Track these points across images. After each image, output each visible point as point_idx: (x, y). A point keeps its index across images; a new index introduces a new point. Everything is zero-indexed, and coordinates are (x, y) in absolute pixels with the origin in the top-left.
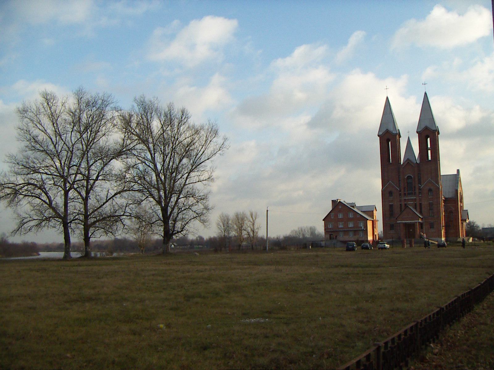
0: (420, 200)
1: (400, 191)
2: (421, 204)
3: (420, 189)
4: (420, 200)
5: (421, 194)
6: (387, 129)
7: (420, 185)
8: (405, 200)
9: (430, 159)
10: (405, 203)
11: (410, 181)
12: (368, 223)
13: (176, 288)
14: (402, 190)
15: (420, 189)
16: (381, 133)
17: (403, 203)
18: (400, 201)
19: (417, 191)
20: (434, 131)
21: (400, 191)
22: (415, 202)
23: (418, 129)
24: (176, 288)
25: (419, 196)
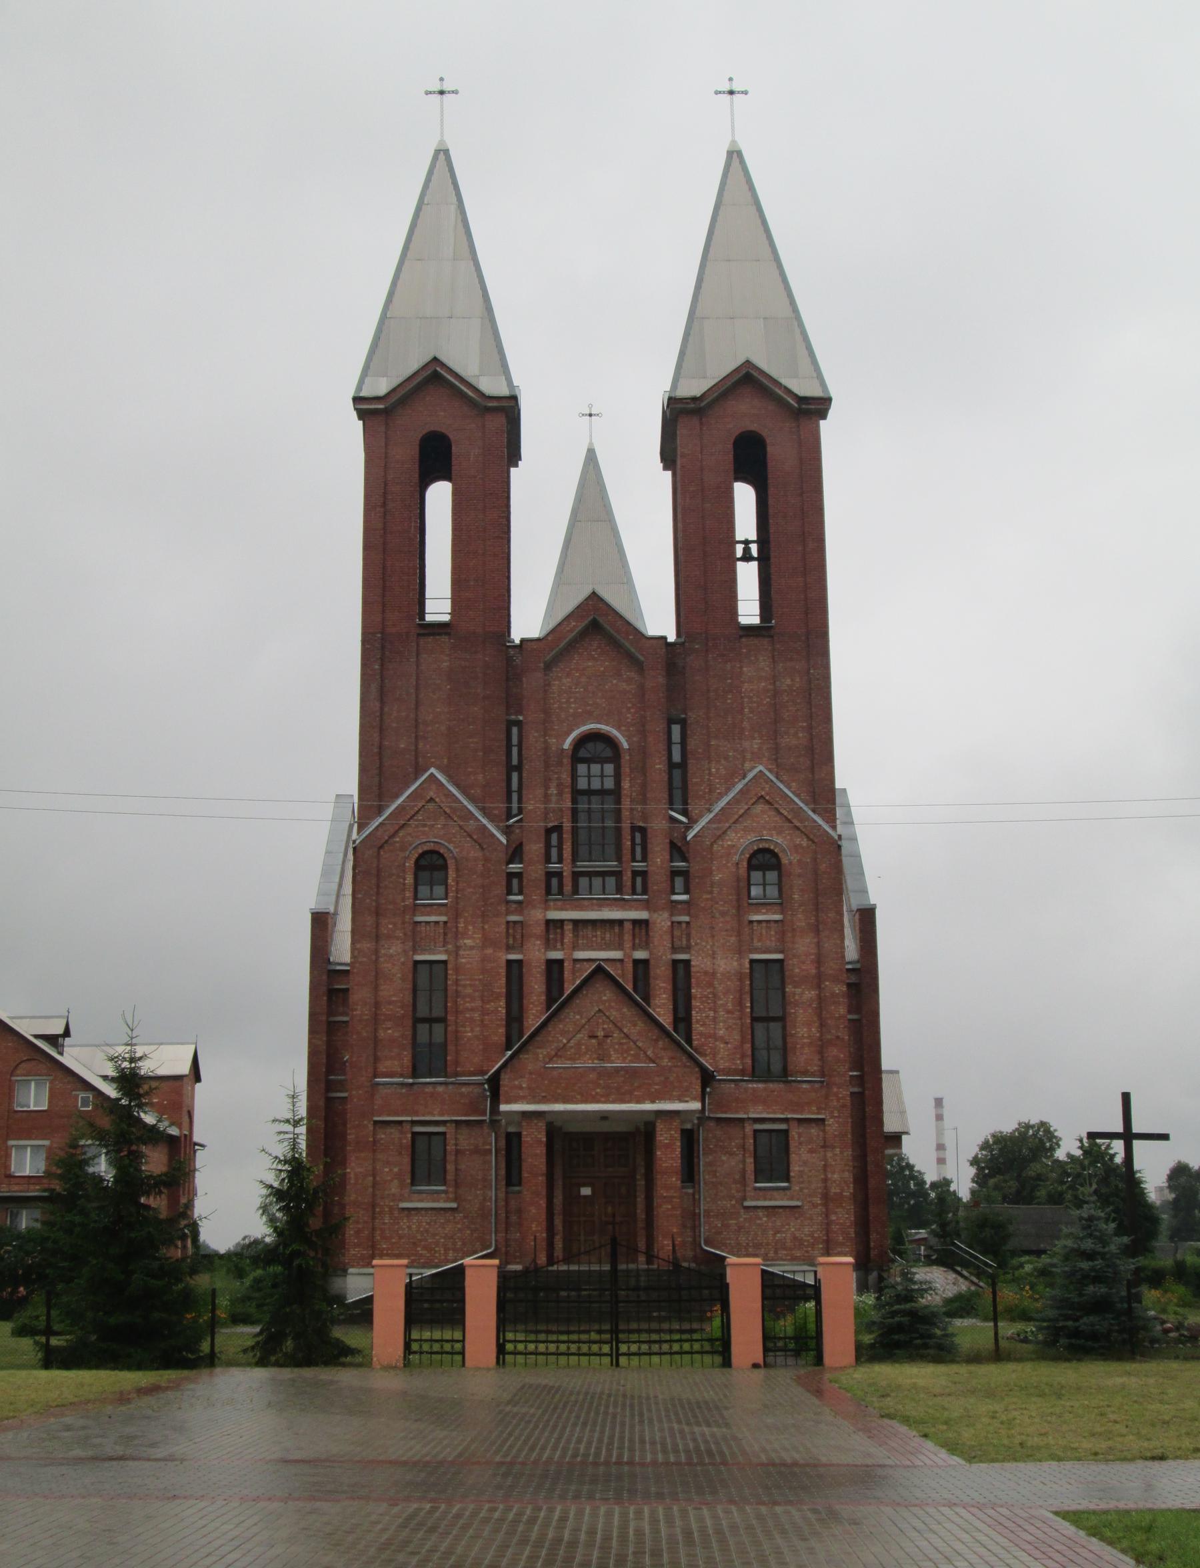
0: (681, 936)
1: (516, 853)
2: (681, 972)
3: (678, 849)
4: (681, 936)
5: (687, 891)
6: (435, 359)
7: (685, 813)
8: (554, 926)
9: (756, 620)
10: (556, 955)
11: (597, 775)
12: (349, 955)
13: (610, 1209)
14: (534, 848)
15: (678, 849)
16: (381, 386)
17: (536, 954)
18: (516, 934)
19: (659, 859)
20: (186, 1119)
21: (516, 853)
22: (640, 955)
23: (682, 382)
24: (610, 1209)
25: (673, 906)
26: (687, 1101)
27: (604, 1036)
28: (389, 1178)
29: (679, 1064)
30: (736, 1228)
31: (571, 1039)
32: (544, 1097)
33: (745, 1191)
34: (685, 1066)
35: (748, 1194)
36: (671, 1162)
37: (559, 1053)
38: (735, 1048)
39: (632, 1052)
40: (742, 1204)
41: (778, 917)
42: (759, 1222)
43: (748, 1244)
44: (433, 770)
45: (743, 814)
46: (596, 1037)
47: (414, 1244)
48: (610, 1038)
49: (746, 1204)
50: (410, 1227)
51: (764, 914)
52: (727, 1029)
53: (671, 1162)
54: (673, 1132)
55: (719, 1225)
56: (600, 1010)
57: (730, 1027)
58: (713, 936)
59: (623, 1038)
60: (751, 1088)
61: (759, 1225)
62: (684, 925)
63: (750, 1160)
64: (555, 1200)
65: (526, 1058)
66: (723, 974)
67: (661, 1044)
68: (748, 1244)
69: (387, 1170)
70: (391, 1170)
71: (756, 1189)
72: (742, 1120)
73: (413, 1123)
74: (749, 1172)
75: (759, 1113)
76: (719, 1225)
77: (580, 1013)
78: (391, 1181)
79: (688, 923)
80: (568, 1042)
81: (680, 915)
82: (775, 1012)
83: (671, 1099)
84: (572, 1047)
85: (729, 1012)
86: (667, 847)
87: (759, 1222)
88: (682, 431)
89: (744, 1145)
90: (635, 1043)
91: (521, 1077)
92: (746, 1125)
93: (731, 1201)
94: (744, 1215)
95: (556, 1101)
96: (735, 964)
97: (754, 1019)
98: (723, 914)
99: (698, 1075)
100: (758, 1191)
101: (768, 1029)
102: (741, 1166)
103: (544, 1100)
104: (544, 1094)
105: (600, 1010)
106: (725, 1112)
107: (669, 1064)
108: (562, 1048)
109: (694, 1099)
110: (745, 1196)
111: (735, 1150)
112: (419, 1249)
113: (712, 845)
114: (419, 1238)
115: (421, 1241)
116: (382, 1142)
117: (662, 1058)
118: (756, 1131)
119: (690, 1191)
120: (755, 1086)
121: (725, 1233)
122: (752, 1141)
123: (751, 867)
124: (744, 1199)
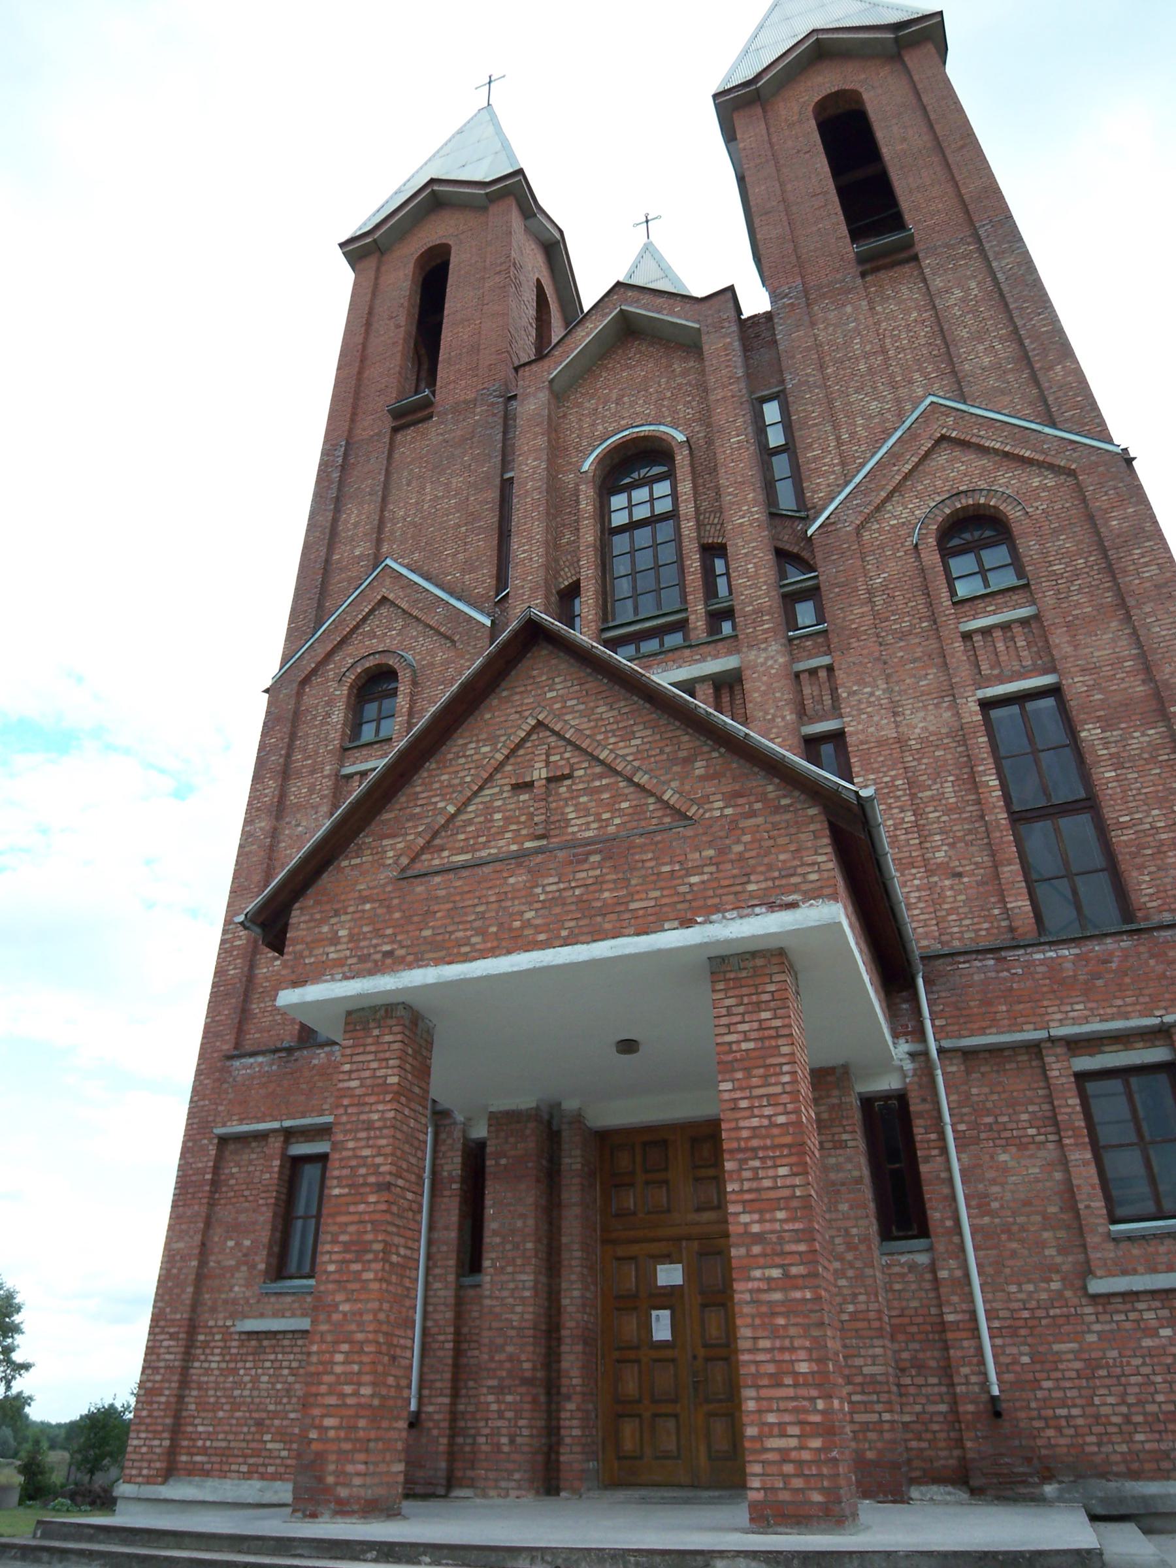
26: (793, 905)
27: (549, 780)
28: (233, 1263)
29: (758, 806)
30: (1078, 1365)
31: (469, 800)
32: (389, 954)
33: (1084, 1246)
34: (778, 809)
35: (1094, 1255)
36: (768, 1111)
37: (437, 842)
38: (981, 883)
39: (624, 805)
40: (1085, 1288)
41: (1024, 612)
42: (1147, 1342)
43: (1127, 1418)
44: (389, 562)
45: (911, 471)
46: (529, 786)
47: (259, 1423)
48: (568, 782)
49: (1097, 1286)
50: (255, 1380)
51: (994, 613)
52: (952, 845)
53: (768, 1111)
54: (765, 1015)
55: (1026, 1359)
56: (540, 724)
57: (961, 839)
58: (888, 676)
59: (601, 776)
60: (1043, 962)
61: (1150, 1353)
62: (823, 674)
63: (1080, 1156)
64: (565, 1302)
65: (354, 867)
66: (920, 739)
67: (699, 767)
68: (1127, 1418)
69: (231, 1243)
70: (237, 1244)
71: (1116, 1240)
72: (1035, 1049)
73: (289, 1135)
74: (1086, 1189)
75: (1075, 1021)
76: (1026, 1359)
77: (492, 740)
78: (237, 1268)
79: (830, 669)
80: (459, 811)
81: (810, 657)
82: (1067, 790)
83: (744, 905)
84: (470, 822)
85: (948, 811)
86: (770, 557)
87: (1147, 1342)
88: (739, 121)
89: (1055, 1116)
90: (630, 780)
91: (337, 913)
92: (1048, 1060)
93: (1049, 1280)
94: (1096, 1328)
95: (418, 961)
96: (947, 715)
97: (1018, 818)
98: (903, 636)
99: (820, 825)
100: (1124, 1245)
101: (1057, 830)
102: (1058, 1176)
103: (390, 962)
104: (387, 948)
105: (540, 724)
106: (982, 1031)
107: (729, 811)
108: (444, 827)
109: (815, 894)
110: (1087, 1262)
111: (1032, 1131)
112: (267, 1437)
113: (860, 528)
114: (271, 1407)
115: (275, 1415)
116: (232, 1182)
117: (706, 799)
118: (1082, 1077)
119: (923, 1259)
120: (1053, 954)
121: (1047, 1384)
122: (1075, 1101)
123: (947, 553)
124: (1087, 1271)
